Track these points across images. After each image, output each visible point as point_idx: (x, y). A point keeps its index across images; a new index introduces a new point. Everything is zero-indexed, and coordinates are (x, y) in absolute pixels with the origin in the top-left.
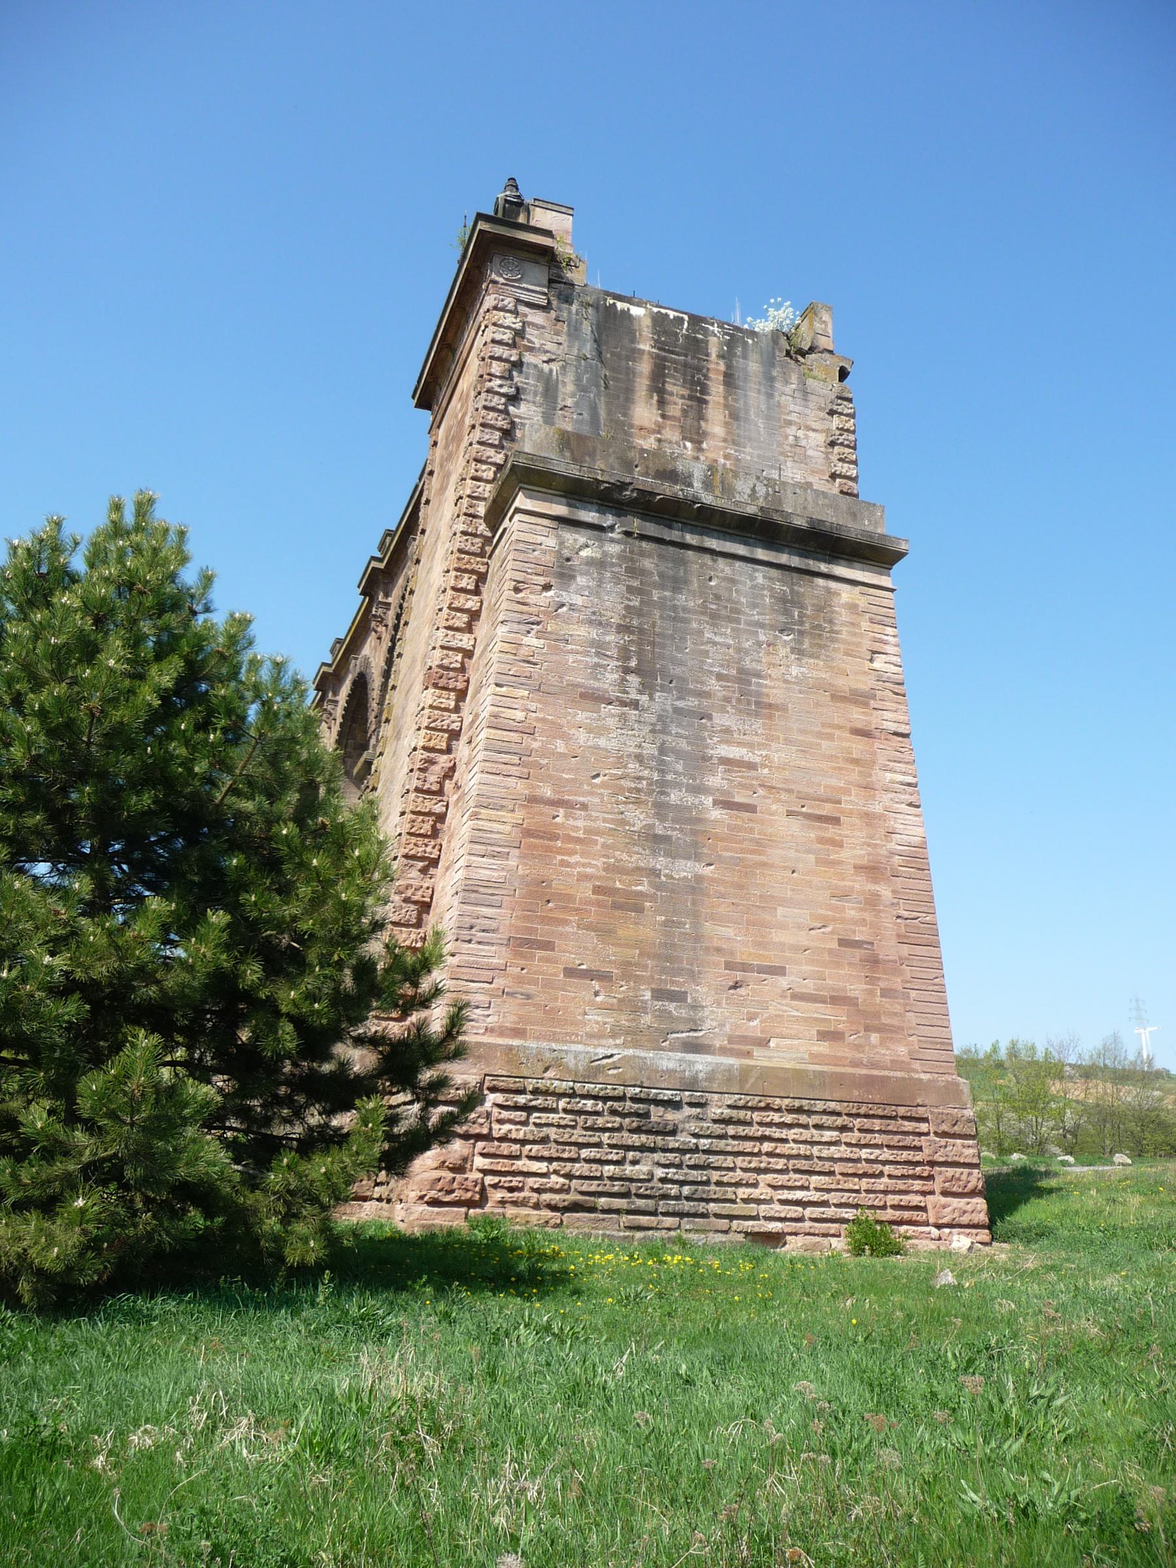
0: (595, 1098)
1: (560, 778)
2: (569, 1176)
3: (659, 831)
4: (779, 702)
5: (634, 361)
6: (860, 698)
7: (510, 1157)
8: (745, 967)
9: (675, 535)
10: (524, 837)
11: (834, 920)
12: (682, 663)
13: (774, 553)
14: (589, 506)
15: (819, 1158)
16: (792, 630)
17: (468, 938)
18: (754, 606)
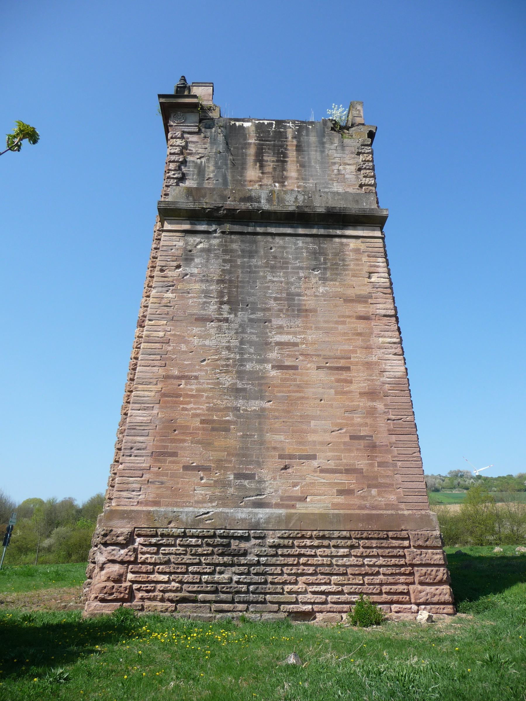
0: (198, 537)
1: (184, 364)
2: (181, 582)
3: (240, 386)
4: (312, 307)
5: (246, 149)
6: (362, 299)
7: (147, 573)
8: (291, 457)
9: (250, 229)
10: (162, 397)
11: (347, 425)
12: (253, 295)
13: (309, 230)
14: (202, 222)
15: (337, 565)
16: (320, 268)
17: (129, 454)
18: (296, 258)
